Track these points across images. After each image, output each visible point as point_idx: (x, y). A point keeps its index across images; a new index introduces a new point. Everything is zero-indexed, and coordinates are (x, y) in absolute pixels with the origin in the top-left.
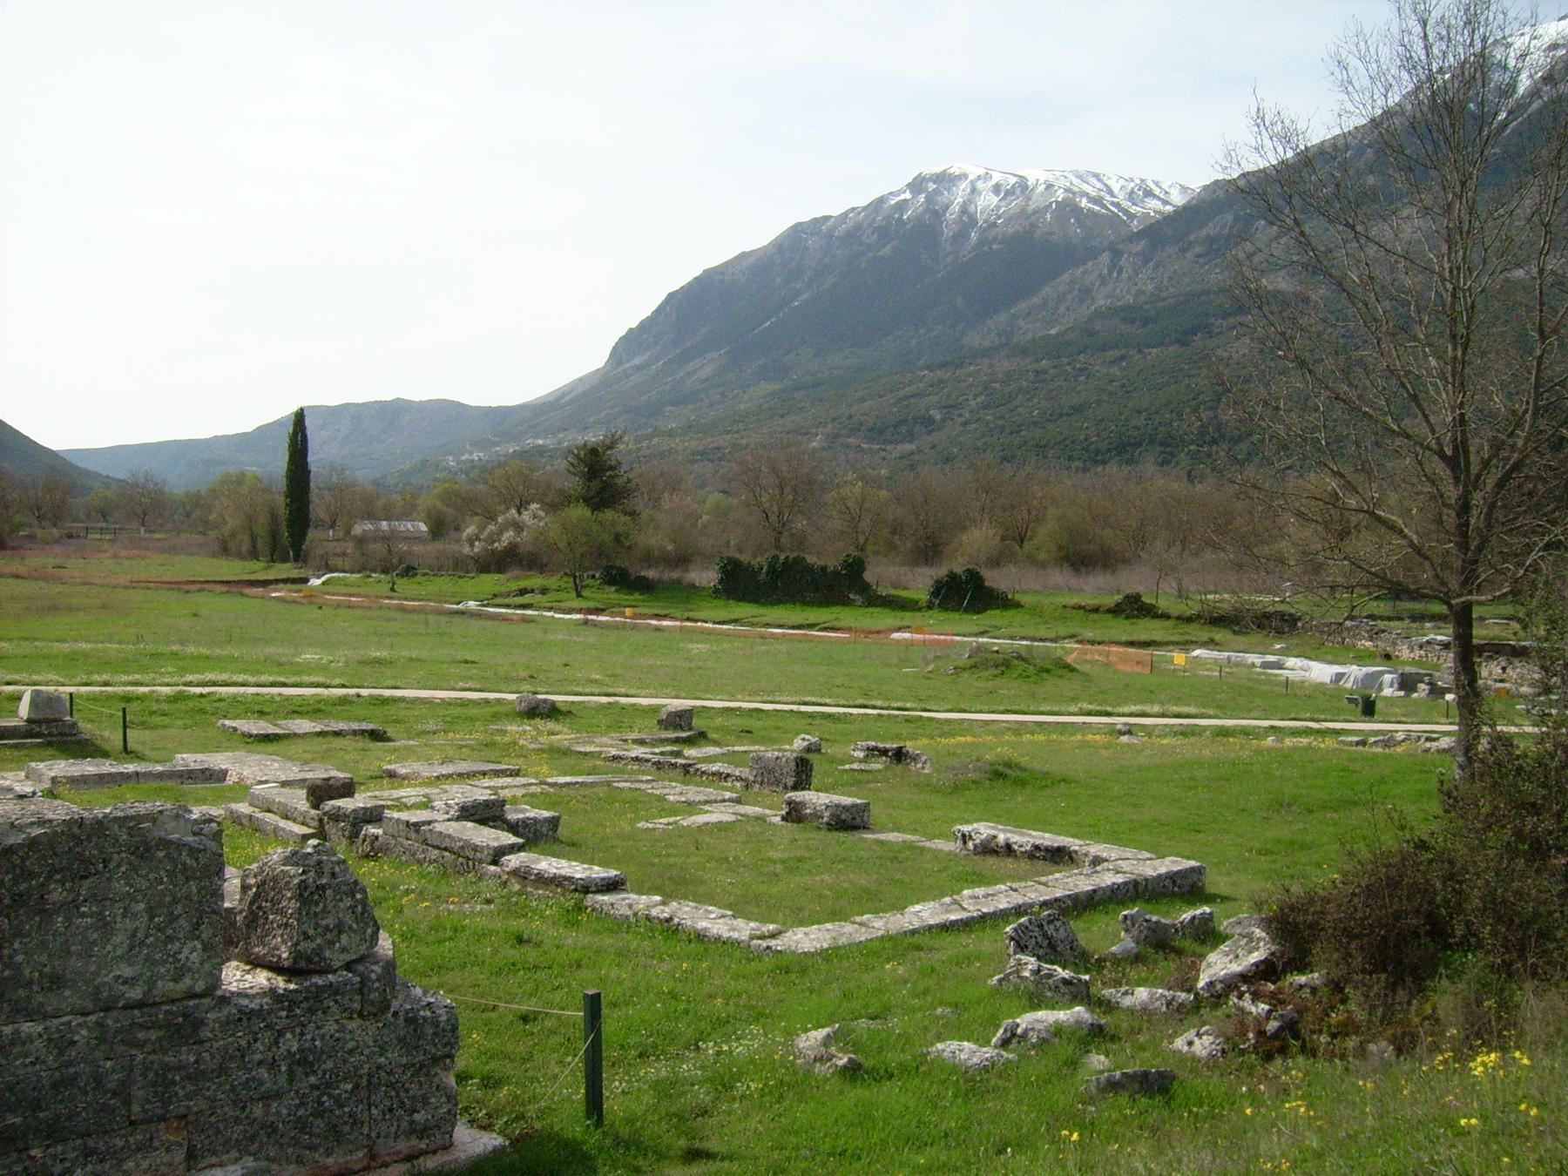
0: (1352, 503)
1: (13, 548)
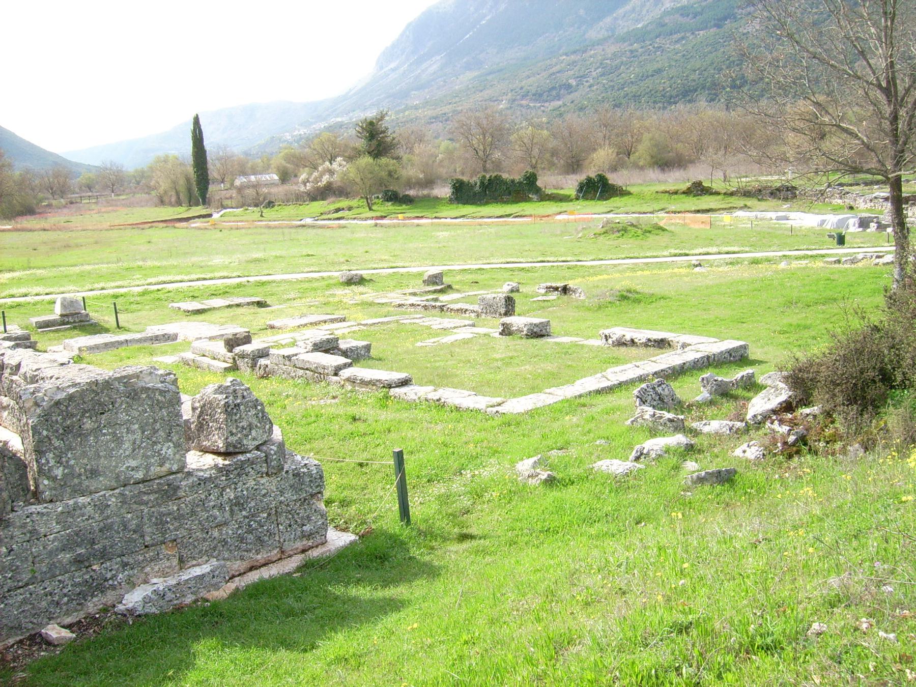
0: (826, 119)
1: (40, 213)
